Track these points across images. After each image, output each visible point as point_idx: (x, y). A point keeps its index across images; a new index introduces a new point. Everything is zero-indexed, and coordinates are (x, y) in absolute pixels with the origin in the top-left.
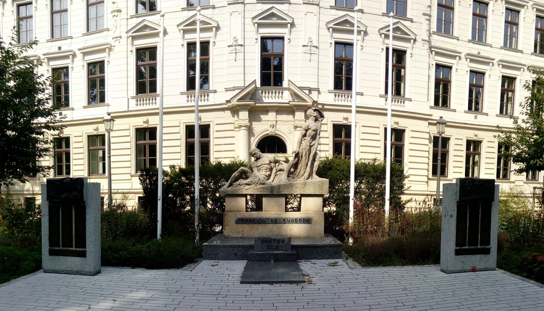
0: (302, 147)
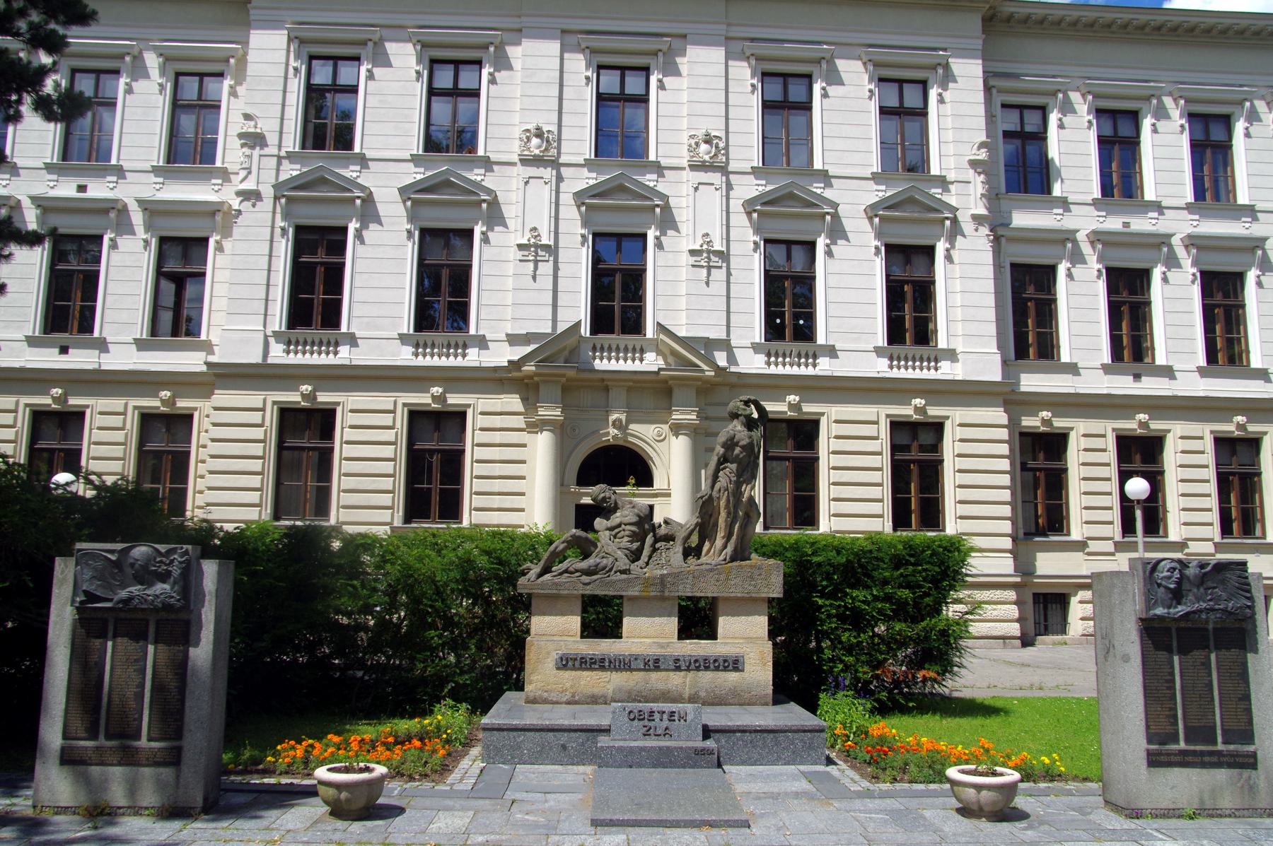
0: (717, 486)
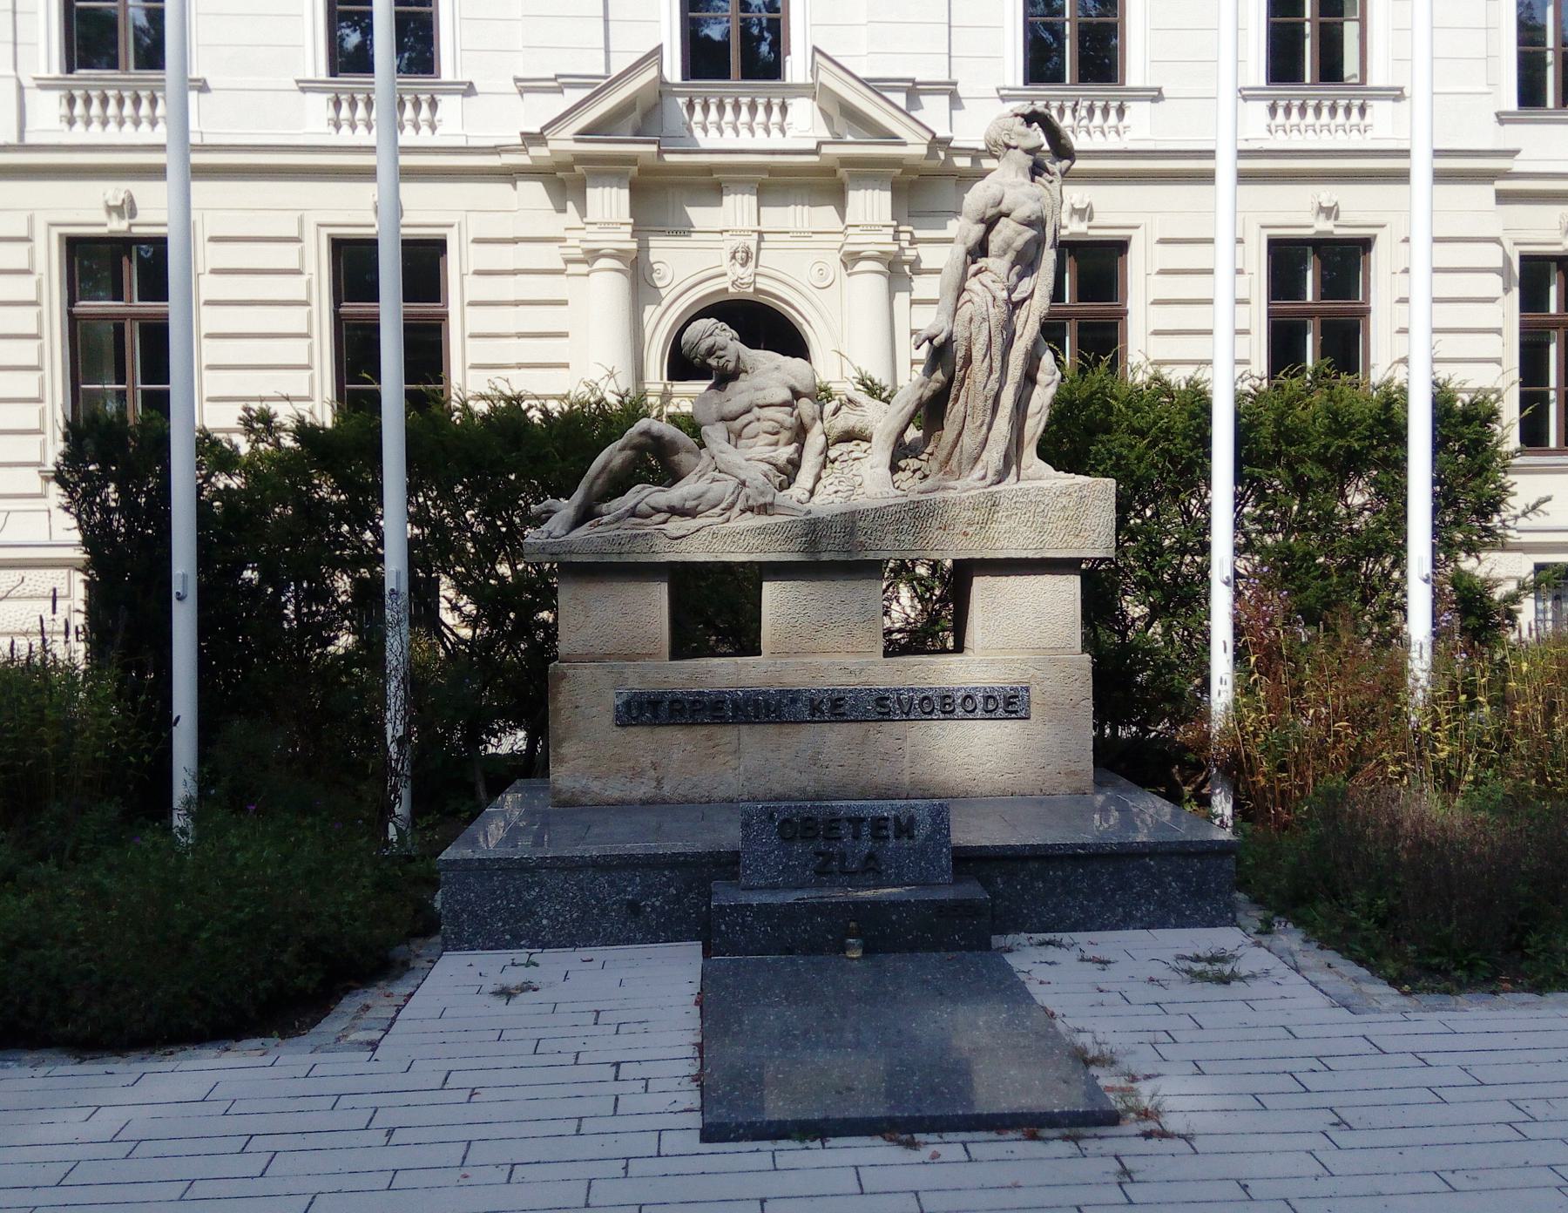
0: (965, 311)
